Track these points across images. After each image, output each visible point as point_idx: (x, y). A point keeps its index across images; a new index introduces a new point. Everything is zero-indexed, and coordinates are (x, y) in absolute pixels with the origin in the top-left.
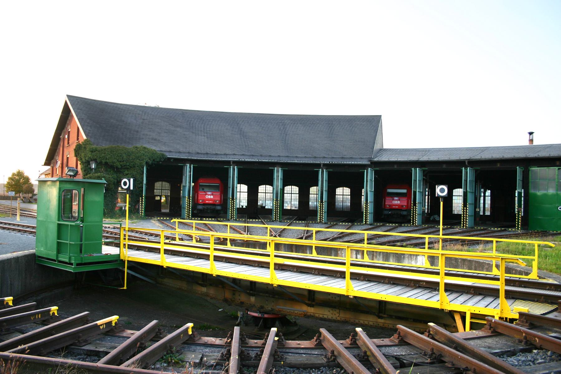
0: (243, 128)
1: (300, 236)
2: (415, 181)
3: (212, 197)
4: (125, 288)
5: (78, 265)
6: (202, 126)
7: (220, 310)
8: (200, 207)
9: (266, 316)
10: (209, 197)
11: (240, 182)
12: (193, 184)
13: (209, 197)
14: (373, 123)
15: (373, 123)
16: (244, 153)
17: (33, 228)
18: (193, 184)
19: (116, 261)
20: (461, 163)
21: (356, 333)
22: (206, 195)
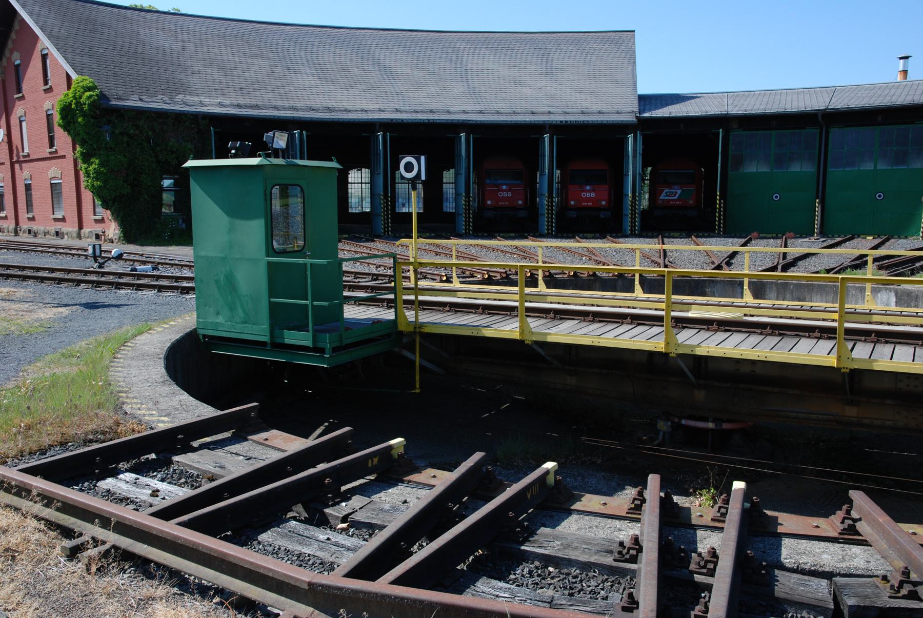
0: (382, 57)
1: (770, 265)
2: (634, 156)
3: (593, 195)
4: (418, 391)
5: (335, 350)
6: (303, 54)
7: (153, 456)
8: (573, 214)
9: (725, 426)
10: (588, 195)
11: (557, 168)
12: (559, 172)
13: (588, 195)
14: (620, 42)
15: (620, 42)
16: (397, 107)
17: (191, 279)
18: (559, 172)
19: (388, 336)
20: (454, 127)
21: (345, 491)
22: (499, 190)
